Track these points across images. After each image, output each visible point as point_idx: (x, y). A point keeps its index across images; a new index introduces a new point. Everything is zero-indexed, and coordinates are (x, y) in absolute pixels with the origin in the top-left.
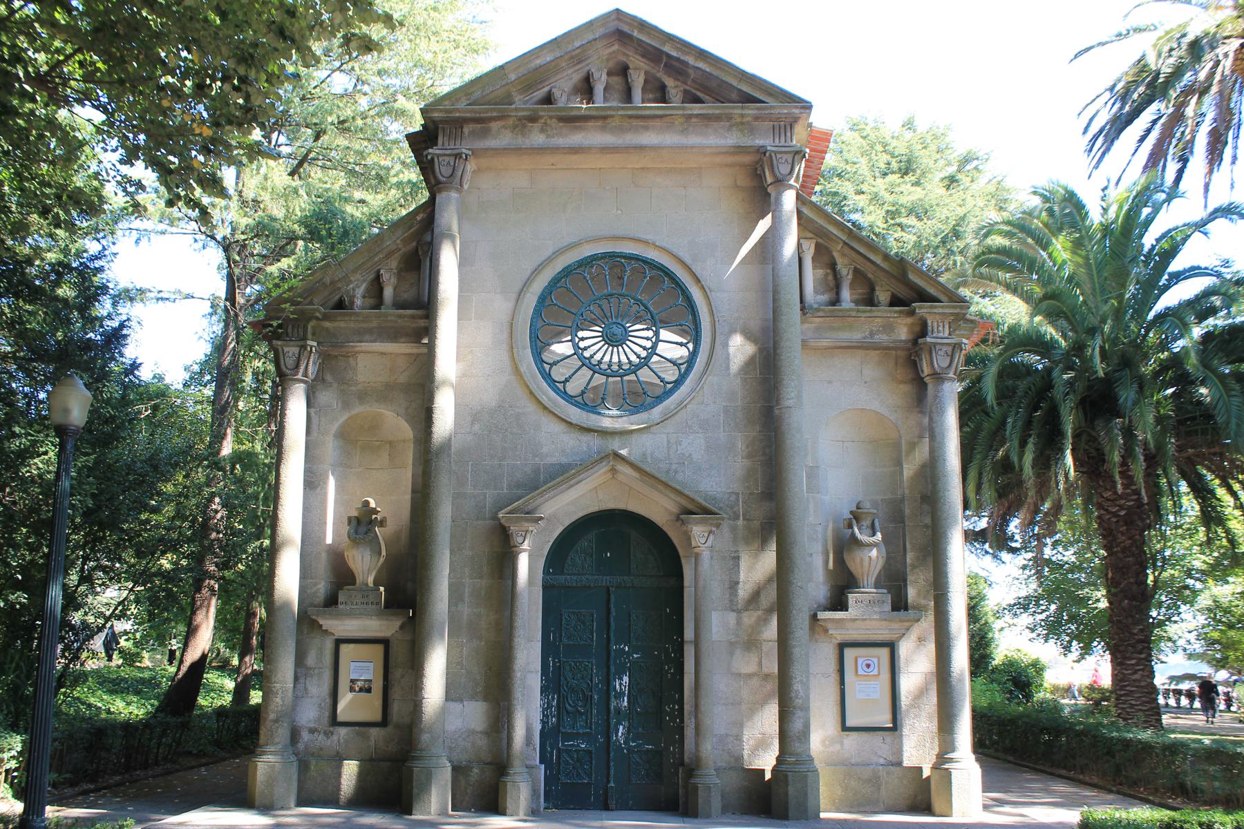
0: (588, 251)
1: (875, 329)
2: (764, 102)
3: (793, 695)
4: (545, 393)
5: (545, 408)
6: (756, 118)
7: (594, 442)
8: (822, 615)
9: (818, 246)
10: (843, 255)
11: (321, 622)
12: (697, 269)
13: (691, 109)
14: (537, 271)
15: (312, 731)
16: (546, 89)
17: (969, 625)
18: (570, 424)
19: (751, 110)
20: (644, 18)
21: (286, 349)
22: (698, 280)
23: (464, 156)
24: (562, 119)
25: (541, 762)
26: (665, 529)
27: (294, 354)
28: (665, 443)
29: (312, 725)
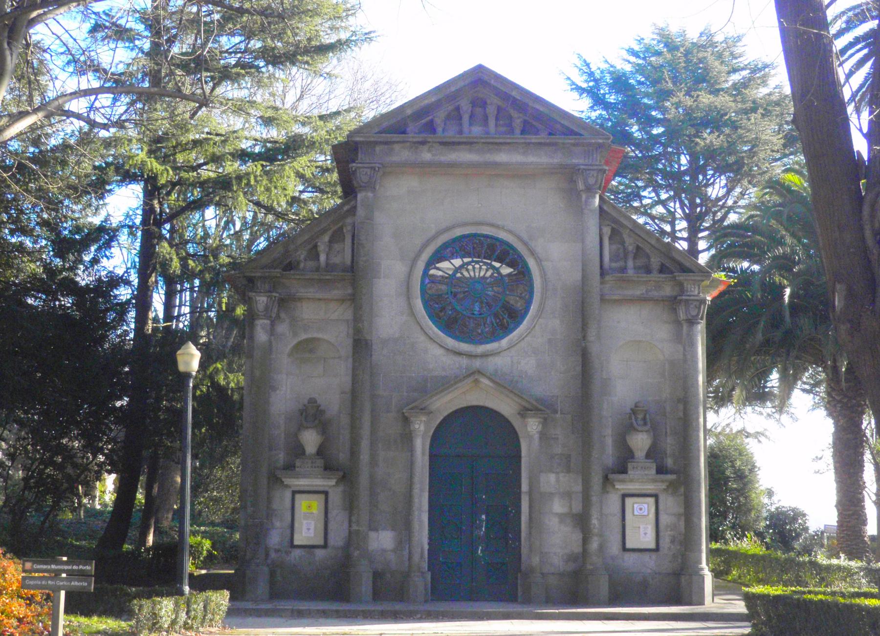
0: (458, 232)
1: (649, 288)
2: (581, 135)
3: (592, 526)
4: (431, 329)
5: (431, 339)
6: (574, 145)
7: (464, 361)
8: (611, 476)
9: (613, 230)
10: (630, 236)
11: (283, 480)
12: (532, 244)
13: (530, 139)
14: (425, 246)
15: (277, 551)
16: (430, 118)
17: (710, 508)
18: (448, 350)
19: (569, 140)
20: (499, 72)
21: (258, 298)
22: (497, 227)
23: (377, 169)
24: (443, 144)
25: (429, 570)
26: (510, 419)
27: (263, 302)
28: (510, 363)
29: (277, 547)
